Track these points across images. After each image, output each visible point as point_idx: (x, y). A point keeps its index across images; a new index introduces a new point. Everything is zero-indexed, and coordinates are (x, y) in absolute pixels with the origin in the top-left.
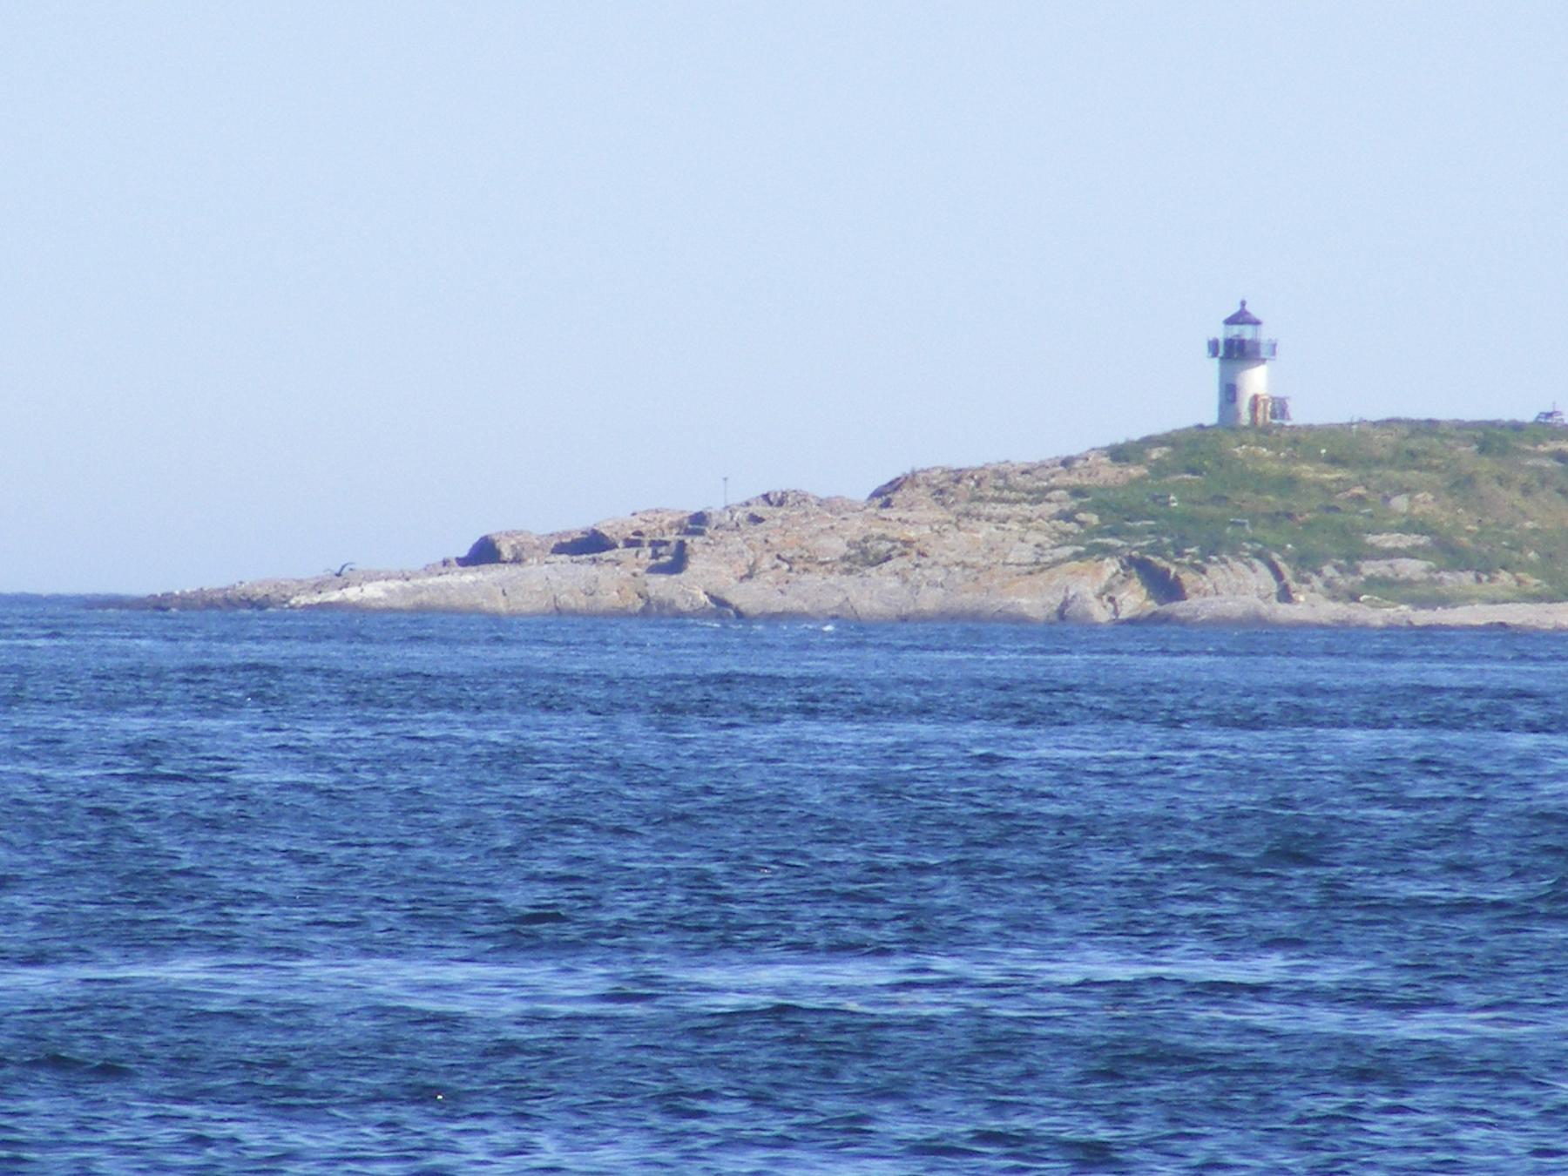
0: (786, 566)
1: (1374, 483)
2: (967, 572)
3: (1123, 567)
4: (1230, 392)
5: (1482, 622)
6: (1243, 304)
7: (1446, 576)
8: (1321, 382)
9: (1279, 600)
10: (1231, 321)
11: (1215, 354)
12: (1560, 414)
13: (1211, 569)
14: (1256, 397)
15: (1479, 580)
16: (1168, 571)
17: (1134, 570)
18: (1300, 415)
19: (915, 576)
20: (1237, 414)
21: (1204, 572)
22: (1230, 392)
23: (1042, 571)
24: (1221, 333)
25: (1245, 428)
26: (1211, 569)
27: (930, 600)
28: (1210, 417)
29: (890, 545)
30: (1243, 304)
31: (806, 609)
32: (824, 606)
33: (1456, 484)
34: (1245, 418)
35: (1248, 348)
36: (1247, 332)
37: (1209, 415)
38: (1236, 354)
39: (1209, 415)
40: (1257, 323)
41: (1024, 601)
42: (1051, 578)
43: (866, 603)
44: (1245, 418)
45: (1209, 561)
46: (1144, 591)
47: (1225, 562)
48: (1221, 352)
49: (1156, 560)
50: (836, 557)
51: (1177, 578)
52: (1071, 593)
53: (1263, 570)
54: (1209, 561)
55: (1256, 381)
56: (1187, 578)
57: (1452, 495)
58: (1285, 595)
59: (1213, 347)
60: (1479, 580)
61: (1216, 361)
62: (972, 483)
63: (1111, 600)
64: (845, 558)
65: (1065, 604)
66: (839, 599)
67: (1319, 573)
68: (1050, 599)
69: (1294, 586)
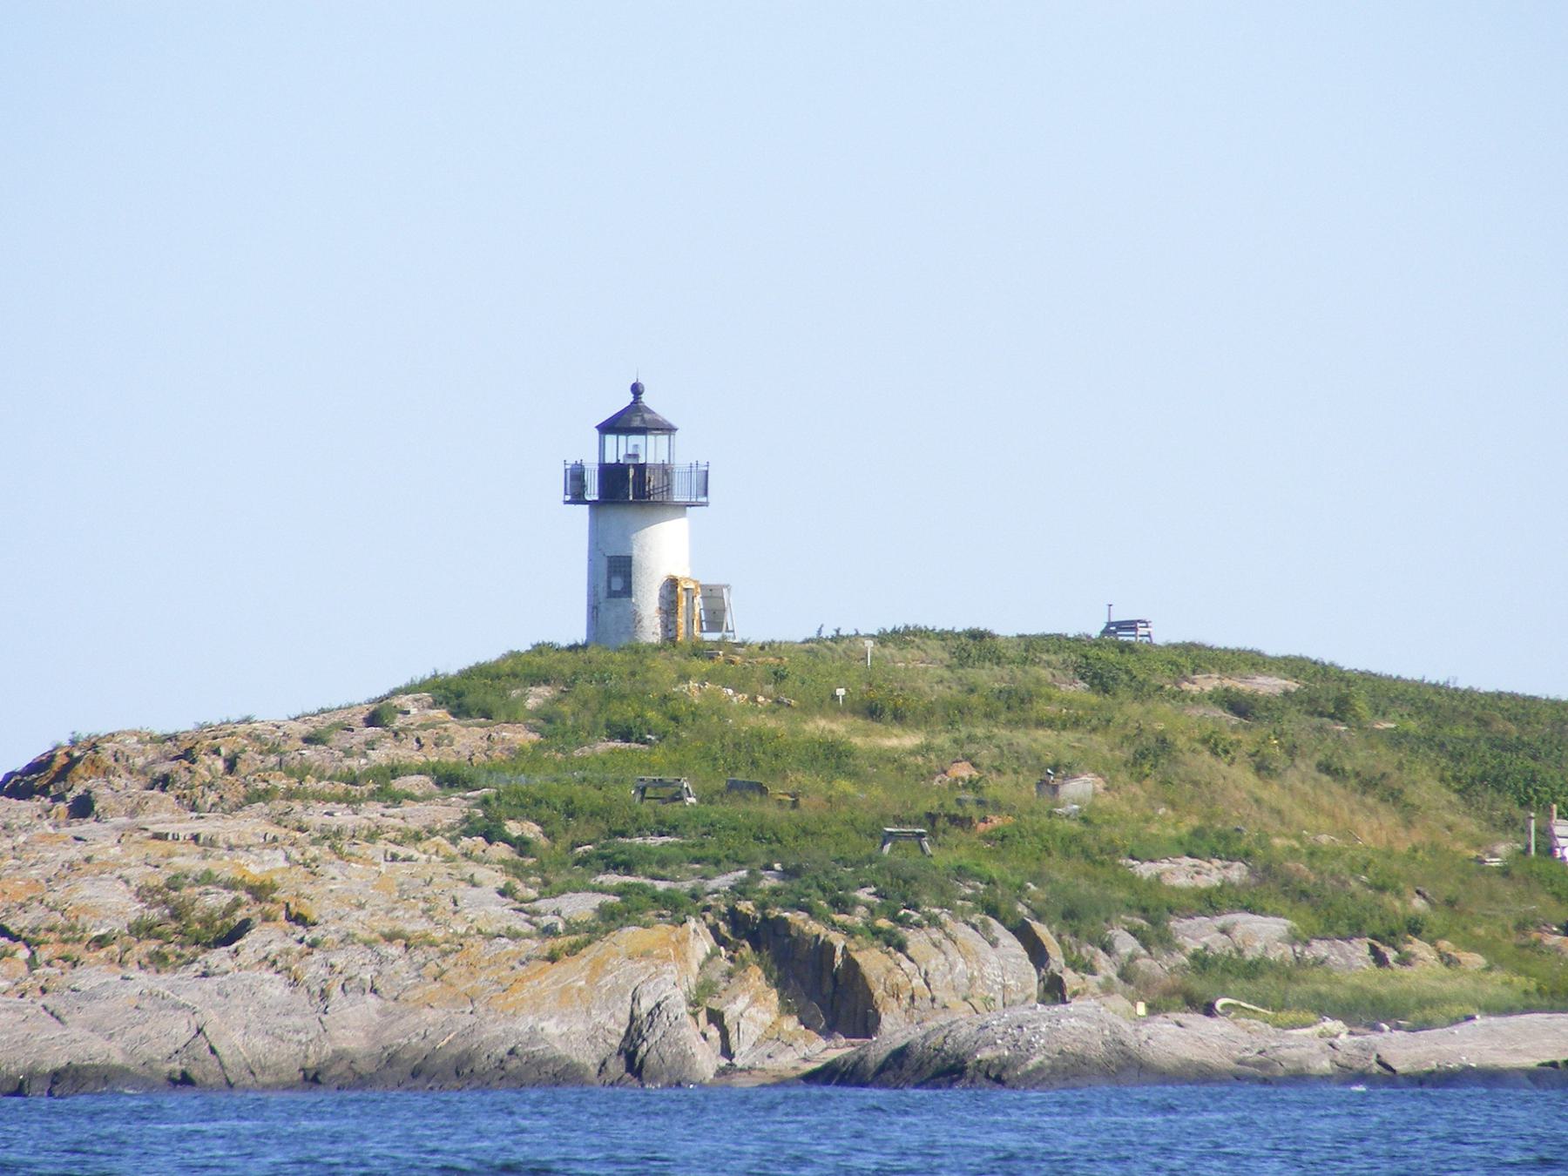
0: (23, 953)
1: (986, 755)
2: (419, 957)
3: (721, 941)
4: (614, 575)
5: (1530, 1062)
6: (636, 390)
7: (1320, 948)
8: (786, 558)
9: (1043, 1002)
10: (613, 426)
11: (577, 497)
12: (1146, 624)
13: (916, 940)
14: (672, 583)
15: (1380, 960)
16: (831, 948)
17: (746, 949)
18: (755, 621)
19: (313, 969)
20: (634, 620)
21: (901, 947)
22: (614, 575)
23: (574, 950)
24: (588, 452)
25: (658, 649)
26: (916, 940)
27: (354, 1028)
28: (570, 627)
29: (227, 897)
30: (636, 390)
31: (118, 1059)
32: (146, 1051)
33: (1142, 755)
34: (651, 629)
35: (654, 481)
36: (651, 450)
37: (565, 621)
38: (623, 491)
39: (565, 621)
40: (669, 430)
41: (551, 1027)
42: (598, 968)
43: (237, 1038)
44: (651, 629)
45: (903, 922)
46: (774, 995)
47: (934, 921)
48: (592, 493)
49: (797, 918)
50: (119, 926)
51: (851, 965)
52: (646, 1004)
53: (1011, 945)
54: (903, 922)
55: (666, 549)
56: (873, 961)
57: (1141, 779)
58: (1054, 991)
59: (576, 478)
60: (1380, 960)
61: (584, 509)
62: (220, 765)
63: (716, 1018)
64: (141, 930)
65: (634, 1033)
66: (181, 1029)
67: (1107, 948)
68: (601, 1017)
69: (1071, 978)
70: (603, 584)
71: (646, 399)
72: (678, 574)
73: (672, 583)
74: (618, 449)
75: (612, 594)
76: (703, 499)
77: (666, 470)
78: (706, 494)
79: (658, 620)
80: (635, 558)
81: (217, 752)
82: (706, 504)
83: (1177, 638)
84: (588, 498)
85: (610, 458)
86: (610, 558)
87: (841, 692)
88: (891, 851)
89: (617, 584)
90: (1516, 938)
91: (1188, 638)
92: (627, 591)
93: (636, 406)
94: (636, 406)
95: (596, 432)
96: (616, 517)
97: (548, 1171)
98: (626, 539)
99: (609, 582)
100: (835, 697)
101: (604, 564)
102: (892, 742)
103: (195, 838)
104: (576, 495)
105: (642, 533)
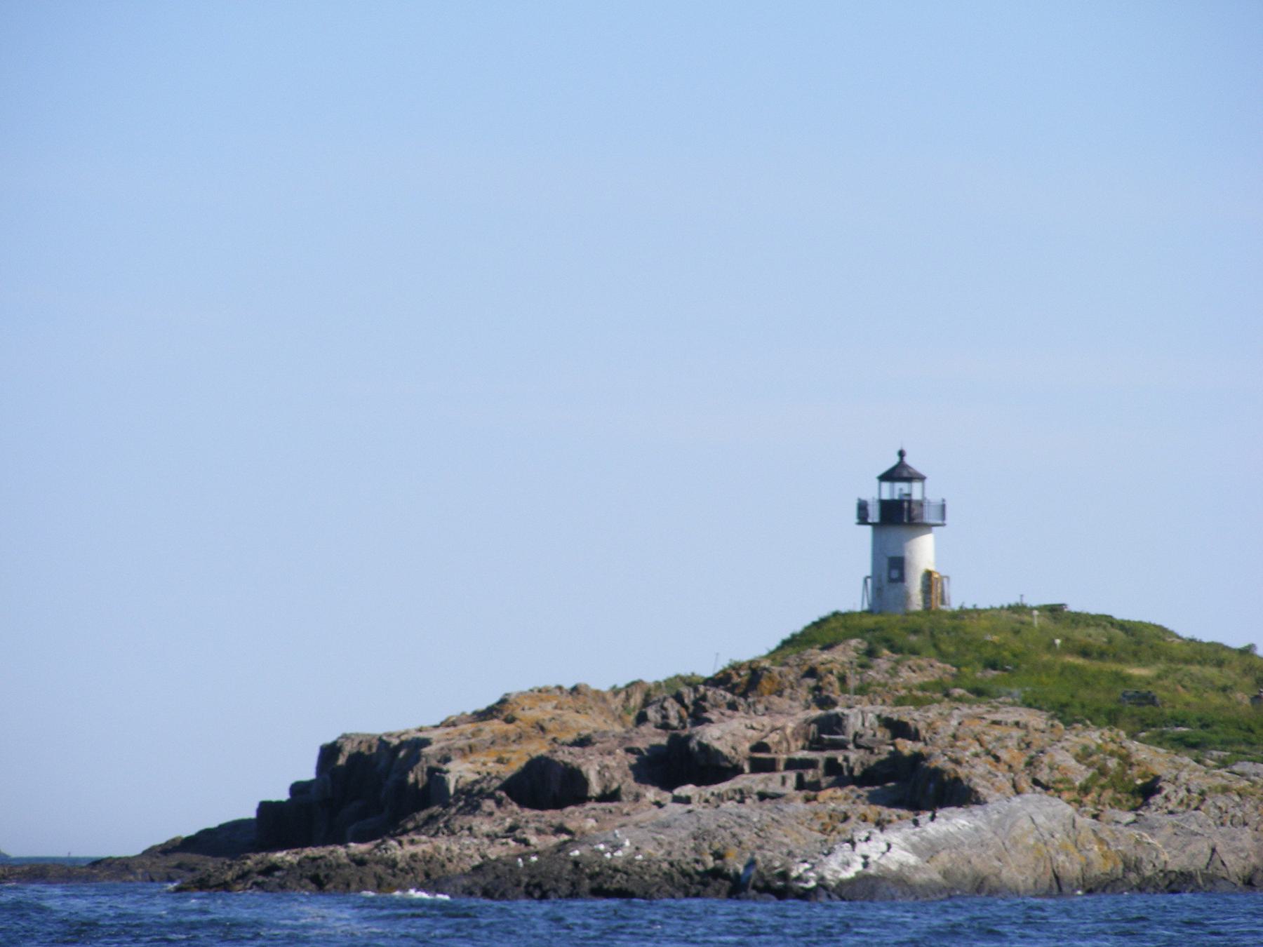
4: (891, 569)
6: (901, 454)
20: (906, 597)
22: (891, 569)
24: (875, 492)
30: (901, 454)
36: (916, 491)
40: (922, 478)
55: (925, 552)
59: (862, 508)
61: (869, 529)
70: (885, 576)
71: (907, 460)
72: (931, 568)
73: (928, 575)
74: (890, 491)
75: (892, 580)
77: (921, 504)
81: (831, 672)
82: (943, 525)
85: (886, 496)
87: (1058, 641)
90: (466, 826)
91: (1108, 613)
92: (902, 578)
93: (901, 465)
94: (901, 465)
95: (877, 481)
96: (893, 533)
97: (306, 940)
98: (902, 548)
99: (889, 573)
100: (1054, 644)
101: (885, 563)
103: (1017, 724)
104: (863, 518)
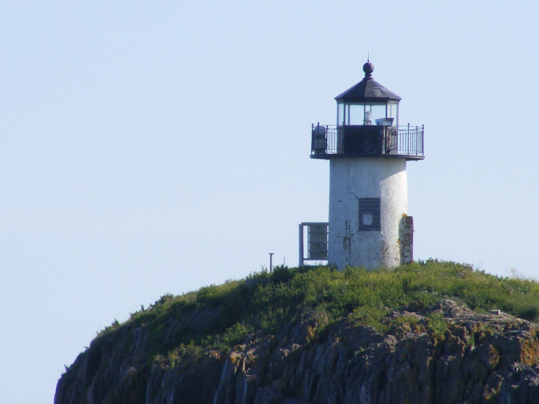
6: (368, 68)
20: (383, 248)
24: (330, 117)
30: (368, 68)
40: (397, 100)
48: (332, 148)
59: (319, 136)
61: (327, 163)
71: (375, 76)
74: (357, 115)
75: (362, 228)
76: (421, 155)
78: (423, 152)
79: (398, 249)
80: (382, 200)
83: (444, 256)
84: (329, 152)
86: (360, 199)
88: (496, 390)
89: (368, 220)
92: (377, 225)
93: (367, 81)
94: (367, 81)
96: (362, 170)
98: (376, 184)
102: (148, 389)
104: (319, 149)
105: (387, 180)
